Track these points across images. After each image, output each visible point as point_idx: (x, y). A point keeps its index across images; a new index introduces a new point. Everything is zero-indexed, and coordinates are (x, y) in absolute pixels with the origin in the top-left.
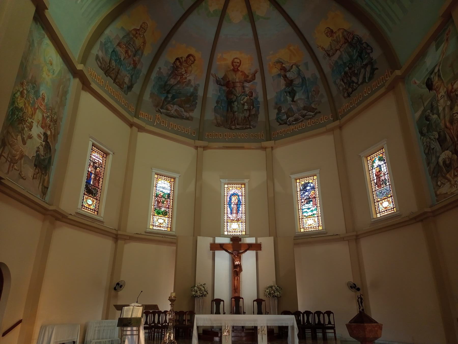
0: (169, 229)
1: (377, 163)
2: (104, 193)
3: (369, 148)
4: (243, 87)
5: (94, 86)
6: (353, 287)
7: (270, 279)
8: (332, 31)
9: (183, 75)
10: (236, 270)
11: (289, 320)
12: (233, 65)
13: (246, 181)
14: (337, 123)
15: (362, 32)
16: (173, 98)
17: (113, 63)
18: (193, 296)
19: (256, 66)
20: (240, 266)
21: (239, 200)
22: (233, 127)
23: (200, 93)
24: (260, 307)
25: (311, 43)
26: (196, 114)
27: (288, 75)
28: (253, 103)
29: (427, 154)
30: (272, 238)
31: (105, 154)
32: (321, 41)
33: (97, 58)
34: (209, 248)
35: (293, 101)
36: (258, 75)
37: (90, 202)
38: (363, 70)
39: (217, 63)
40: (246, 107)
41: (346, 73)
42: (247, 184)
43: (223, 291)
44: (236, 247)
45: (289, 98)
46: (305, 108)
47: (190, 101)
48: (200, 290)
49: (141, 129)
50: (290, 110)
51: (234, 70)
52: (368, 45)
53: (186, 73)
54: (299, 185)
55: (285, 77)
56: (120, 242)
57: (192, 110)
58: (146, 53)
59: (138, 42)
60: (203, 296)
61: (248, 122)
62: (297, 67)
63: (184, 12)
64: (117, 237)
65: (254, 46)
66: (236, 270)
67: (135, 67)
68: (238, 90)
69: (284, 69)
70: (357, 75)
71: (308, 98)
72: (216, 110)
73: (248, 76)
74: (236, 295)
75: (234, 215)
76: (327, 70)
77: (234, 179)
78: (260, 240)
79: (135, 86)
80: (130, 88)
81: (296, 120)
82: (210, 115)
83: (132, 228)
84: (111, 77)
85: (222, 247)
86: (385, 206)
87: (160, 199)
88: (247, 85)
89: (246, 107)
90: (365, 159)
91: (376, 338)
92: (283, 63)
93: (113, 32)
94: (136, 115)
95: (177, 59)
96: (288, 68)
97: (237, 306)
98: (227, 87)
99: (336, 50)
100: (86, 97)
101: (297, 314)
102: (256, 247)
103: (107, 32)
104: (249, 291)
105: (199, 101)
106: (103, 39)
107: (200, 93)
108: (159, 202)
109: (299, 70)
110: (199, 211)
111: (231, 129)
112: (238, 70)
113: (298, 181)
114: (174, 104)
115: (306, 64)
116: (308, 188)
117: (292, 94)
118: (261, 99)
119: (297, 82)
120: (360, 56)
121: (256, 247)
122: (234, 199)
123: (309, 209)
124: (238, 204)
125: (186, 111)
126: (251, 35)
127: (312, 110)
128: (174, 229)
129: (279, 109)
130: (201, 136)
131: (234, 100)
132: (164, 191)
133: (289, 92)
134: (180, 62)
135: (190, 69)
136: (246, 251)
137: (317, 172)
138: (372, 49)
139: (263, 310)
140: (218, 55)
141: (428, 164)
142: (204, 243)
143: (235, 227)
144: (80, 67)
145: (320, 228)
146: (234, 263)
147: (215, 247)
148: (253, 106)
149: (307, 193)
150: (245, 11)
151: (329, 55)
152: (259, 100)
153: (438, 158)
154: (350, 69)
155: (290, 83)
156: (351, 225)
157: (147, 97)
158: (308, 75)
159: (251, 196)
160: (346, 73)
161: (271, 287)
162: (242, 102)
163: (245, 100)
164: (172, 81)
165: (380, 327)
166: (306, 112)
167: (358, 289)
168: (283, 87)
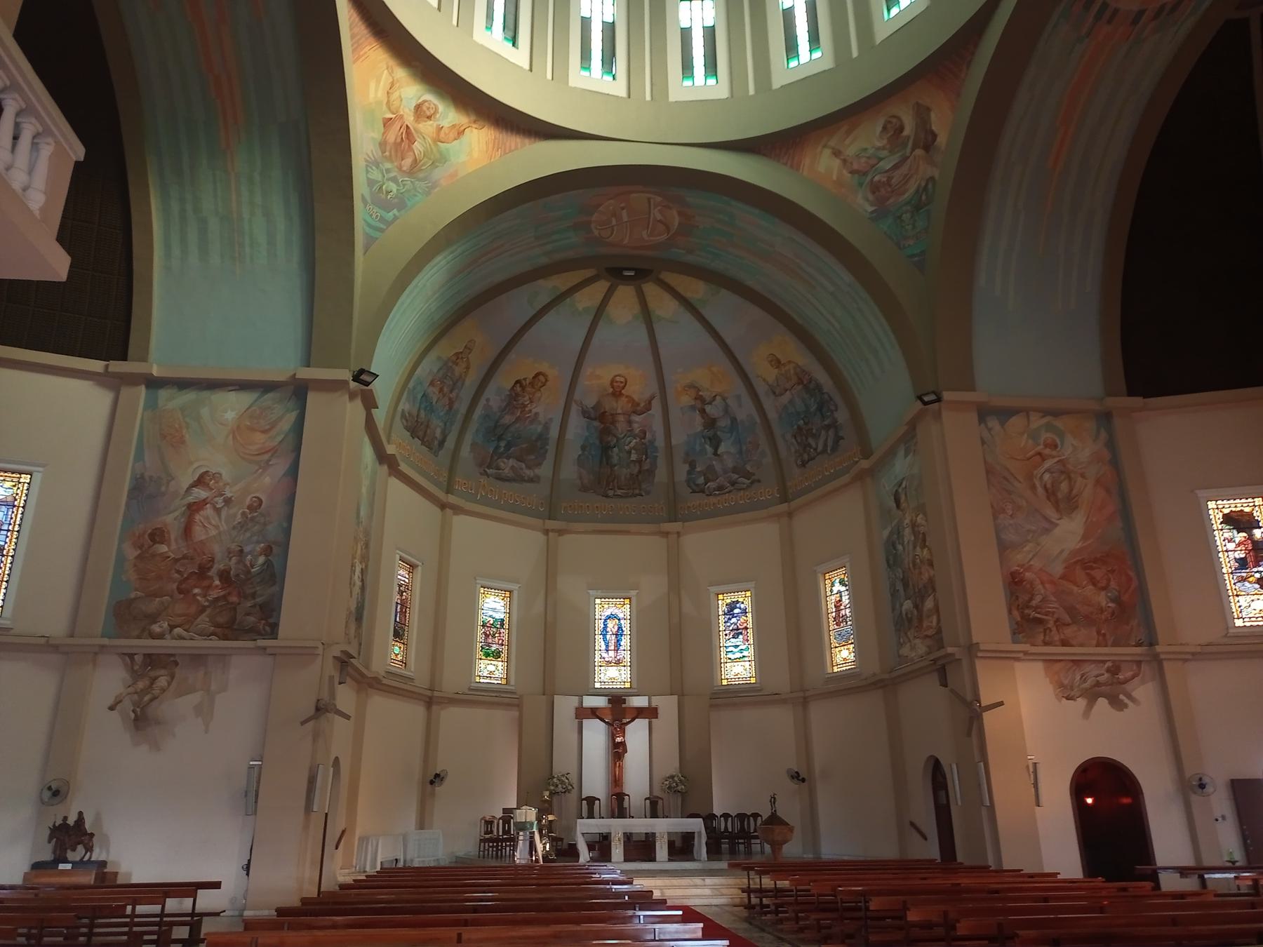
0: (504, 682)
1: (837, 587)
2: (413, 633)
3: (828, 561)
4: (630, 422)
5: (404, 467)
6: (796, 777)
7: (670, 765)
8: (779, 361)
10: (617, 751)
11: (696, 825)
13: (633, 593)
14: (784, 507)
15: (821, 376)
16: (508, 446)
17: (423, 414)
18: (548, 787)
19: (654, 388)
20: (623, 744)
21: (620, 628)
22: (611, 493)
23: (554, 433)
24: (654, 808)
25: (747, 368)
26: (545, 470)
27: (708, 408)
28: (646, 450)
29: (892, 595)
30: (674, 699)
31: (412, 567)
32: (763, 372)
33: (403, 416)
34: (573, 716)
35: (715, 454)
36: (656, 405)
37: (397, 650)
38: (823, 432)
39: (584, 381)
40: (634, 457)
41: (799, 428)
42: (634, 599)
43: (595, 782)
44: (618, 711)
45: (709, 449)
46: (735, 470)
47: (535, 448)
48: (562, 782)
49: (457, 510)
50: (710, 468)
51: (614, 394)
54: (723, 603)
55: (703, 411)
56: (434, 708)
57: (540, 464)
58: (468, 382)
59: (458, 370)
60: (567, 791)
61: (637, 483)
62: (724, 399)
64: (431, 700)
65: (650, 358)
66: (617, 751)
67: (451, 408)
68: (621, 426)
70: (816, 437)
71: (740, 452)
72: (580, 462)
73: (638, 404)
74: (617, 790)
75: (612, 653)
76: (772, 415)
77: (612, 590)
78: (656, 701)
79: (449, 438)
80: (442, 443)
81: (720, 488)
82: (569, 471)
83: (450, 683)
85: (594, 713)
86: (843, 656)
87: (492, 629)
88: (636, 418)
89: (634, 457)
90: (821, 578)
91: (785, 842)
93: (429, 366)
95: (517, 382)
96: (708, 399)
97: (619, 806)
100: (395, 484)
101: (709, 818)
102: (649, 713)
103: (419, 369)
104: (637, 782)
105: (551, 448)
106: (411, 385)
107: (554, 433)
108: (487, 636)
110: (552, 646)
111: (607, 496)
112: (621, 394)
113: (721, 597)
114: (508, 458)
115: (738, 397)
116: (736, 611)
117: (715, 442)
118: (660, 442)
119: (724, 423)
120: (820, 409)
121: (649, 713)
122: (611, 625)
123: (736, 646)
124: (619, 634)
125: (529, 467)
127: (748, 475)
128: (512, 682)
129: (692, 465)
130: (553, 512)
132: (495, 615)
135: (538, 395)
136: (633, 720)
137: (752, 585)
138: (836, 406)
139: (660, 812)
140: (587, 370)
141: (893, 609)
142: (565, 706)
143: (613, 674)
144: (390, 449)
145: (753, 680)
146: (614, 740)
147: (584, 713)
149: (734, 620)
150: (637, 309)
152: (657, 444)
153: (901, 605)
154: (806, 424)
155: (711, 423)
156: (793, 680)
157: (465, 451)
158: (741, 416)
159: (638, 619)
160: (799, 428)
161: (672, 777)
163: (632, 444)
164: (508, 419)
165: (791, 830)
167: (803, 780)
168: (700, 428)
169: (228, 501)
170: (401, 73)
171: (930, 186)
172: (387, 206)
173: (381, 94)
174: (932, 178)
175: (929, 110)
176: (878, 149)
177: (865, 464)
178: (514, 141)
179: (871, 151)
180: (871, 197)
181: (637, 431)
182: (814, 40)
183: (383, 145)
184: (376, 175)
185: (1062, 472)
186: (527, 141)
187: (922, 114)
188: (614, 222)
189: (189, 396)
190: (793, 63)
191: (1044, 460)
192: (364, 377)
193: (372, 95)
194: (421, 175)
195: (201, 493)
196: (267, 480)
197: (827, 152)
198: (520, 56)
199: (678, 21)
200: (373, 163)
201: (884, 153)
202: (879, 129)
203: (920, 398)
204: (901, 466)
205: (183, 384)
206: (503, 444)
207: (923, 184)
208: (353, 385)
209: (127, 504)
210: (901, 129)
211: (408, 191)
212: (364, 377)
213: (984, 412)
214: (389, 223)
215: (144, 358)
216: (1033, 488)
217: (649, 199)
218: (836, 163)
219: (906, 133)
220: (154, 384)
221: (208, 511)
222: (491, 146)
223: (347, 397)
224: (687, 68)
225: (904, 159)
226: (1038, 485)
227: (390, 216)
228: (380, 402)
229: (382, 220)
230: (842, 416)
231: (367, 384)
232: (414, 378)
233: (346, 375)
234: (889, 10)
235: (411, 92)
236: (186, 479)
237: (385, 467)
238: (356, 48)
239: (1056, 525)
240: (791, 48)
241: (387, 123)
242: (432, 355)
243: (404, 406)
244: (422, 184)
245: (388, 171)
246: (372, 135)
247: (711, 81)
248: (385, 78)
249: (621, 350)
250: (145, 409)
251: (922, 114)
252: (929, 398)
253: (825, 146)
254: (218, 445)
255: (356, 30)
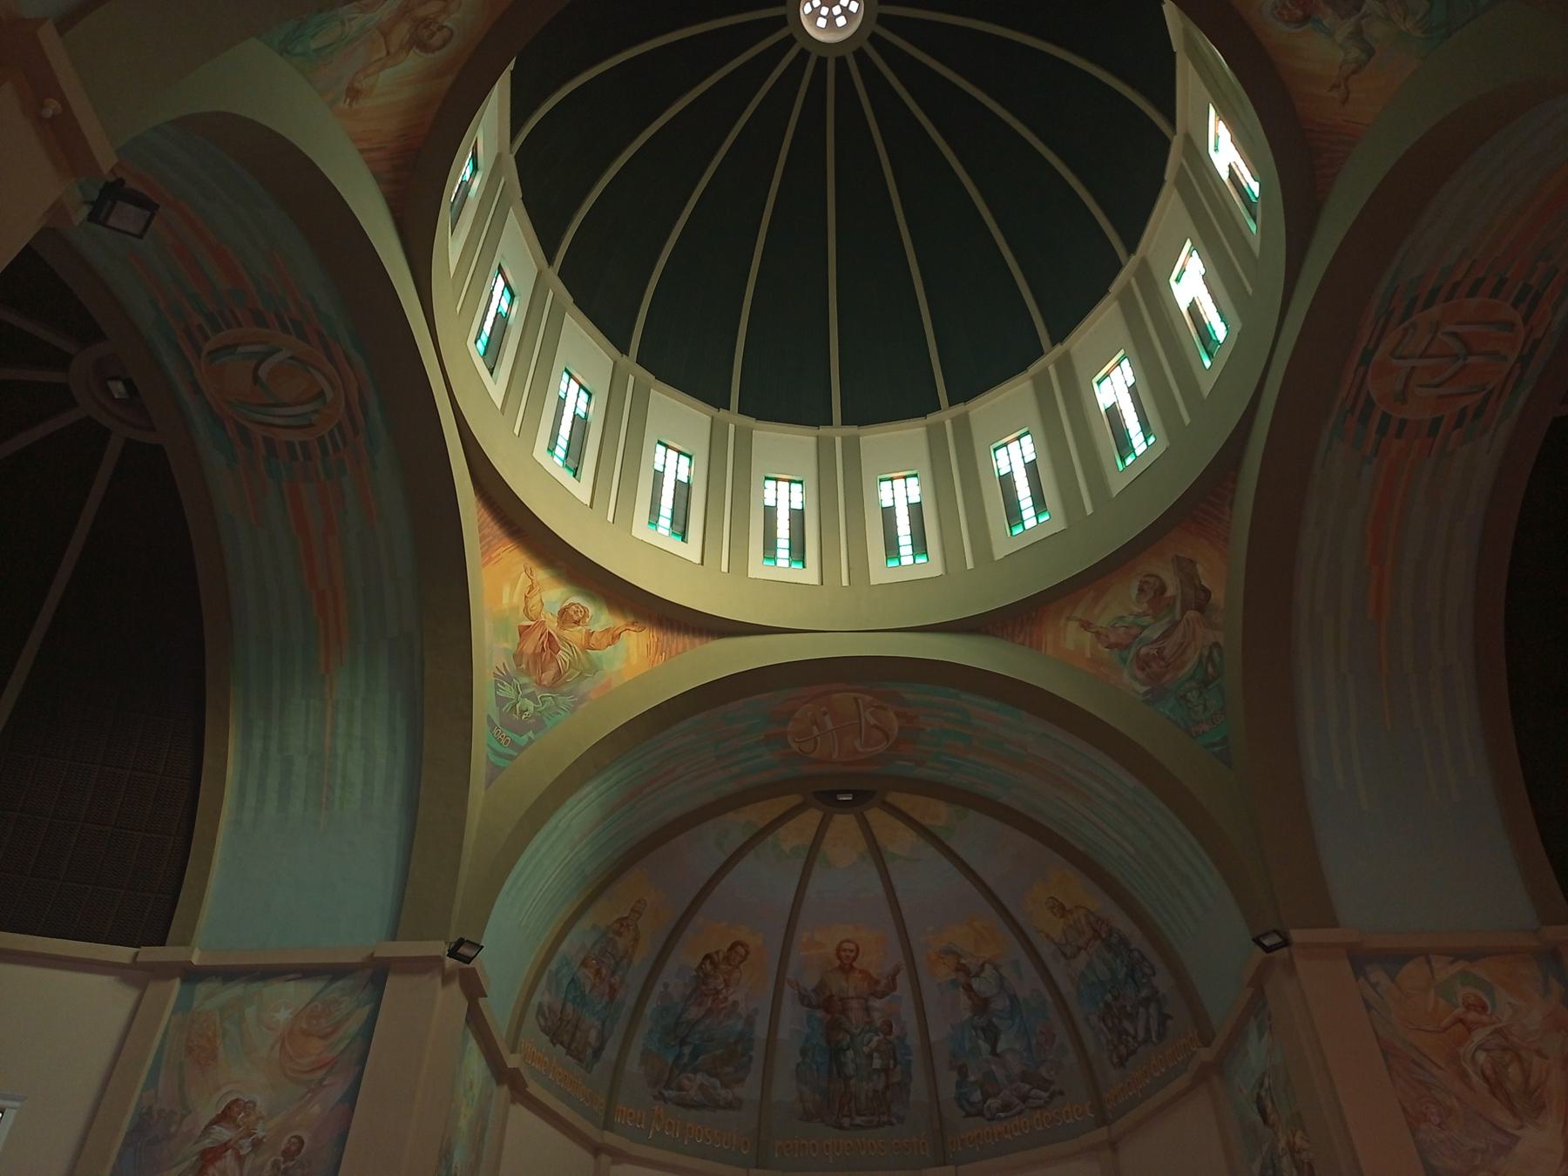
5: (534, 1088)
8: (1062, 907)
9: (718, 992)
12: (839, 958)
14: (1101, 1134)
15: (1123, 924)
16: (695, 1055)
22: (846, 1122)
23: (761, 1030)
26: (749, 1089)
27: (975, 984)
35: (994, 1052)
36: (903, 980)
38: (1141, 1010)
40: (877, 1063)
41: (1107, 1005)
45: (985, 1046)
49: (619, 1156)
51: (841, 968)
52: (1143, 957)
53: (727, 986)
55: (969, 988)
62: (996, 968)
63: (724, 858)
69: (961, 968)
73: (877, 982)
76: (1066, 988)
80: (598, 1052)
81: (1006, 1107)
84: (562, 1044)
88: (876, 1003)
89: (877, 1063)
92: (959, 956)
94: (607, 1125)
95: (707, 957)
98: (827, 1011)
99: (1080, 949)
100: (520, 1113)
106: (553, 966)
107: (761, 1030)
109: (1001, 978)
111: (841, 1127)
112: (852, 967)
114: (695, 1071)
118: (913, 1040)
119: (1000, 1004)
125: (725, 1086)
126: (878, 889)
129: (962, 1072)
131: (844, 1044)
133: (983, 1029)
134: (712, 963)
143: (827, 718)
144: (513, 1061)
148: (895, 1059)
151: (1064, 955)
154: (1116, 998)
155: (982, 1005)
157: (633, 1064)
160: (1107, 1005)
162: (866, 1050)
163: (874, 1044)
164: (694, 1013)
166: (1028, 1087)
168: (967, 1015)
169: (257, 1145)
170: (541, 575)
171: (1215, 654)
172: (520, 728)
173: (518, 599)
174: (1216, 644)
175: (1192, 562)
176: (1138, 615)
177: (1205, 1055)
178: (681, 642)
179: (1131, 619)
180: (1139, 674)
181: (878, 1023)
182: (1039, 503)
183: (518, 656)
184: (508, 692)
185: (1504, 1049)
186: (697, 641)
187: (1186, 569)
188: (816, 731)
189: (236, 990)
190: (1018, 530)
191: (1470, 1030)
192: (463, 950)
193: (505, 601)
194: (565, 689)
195: (223, 1133)
196: (316, 1109)
197: (1073, 626)
198: (581, 490)
199: (878, 501)
200: (503, 678)
201: (1147, 620)
202: (1134, 592)
203: (1257, 941)
204: (1256, 1053)
205: (228, 975)
206: (687, 1050)
207: (1206, 653)
208: (450, 962)
209: (120, 1156)
210: (1163, 589)
211: (549, 708)
212: (463, 950)
213: (1360, 959)
214: (521, 749)
215: (186, 942)
216: (1464, 1076)
217: (856, 699)
218: (1088, 637)
219: (1170, 592)
220: (192, 975)
221: (229, 1160)
222: (653, 650)
223: (439, 980)
224: (892, 548)
225: (1175, 624)
226: (1470, 1070)
227: (525, 738)
228: (491, 990)
229: (513, 745)
230: (1163, 982)
231: (468, 960)
232: (557, 957)
233: (440, 948)
234: (1123, 460)
235: (554, 595)
236: (208, 1112)
237: (506, 1088)
238: (487, 550)
239: (1518, 1138)
240: (1014, 515)
241: (524, 631)
242: (585, 924)
243: (541, 997)
244: (567, 699)
245: (523, 686)
246: (506, 645)
247: (921, 560)
248: (523, 582)
249: (837, 898)
250: (173, 1013)
251: (1186, 569)
252: (1273, 942)
253: (1069, 619)
254: (257, 1059)
255: (486, 531)
